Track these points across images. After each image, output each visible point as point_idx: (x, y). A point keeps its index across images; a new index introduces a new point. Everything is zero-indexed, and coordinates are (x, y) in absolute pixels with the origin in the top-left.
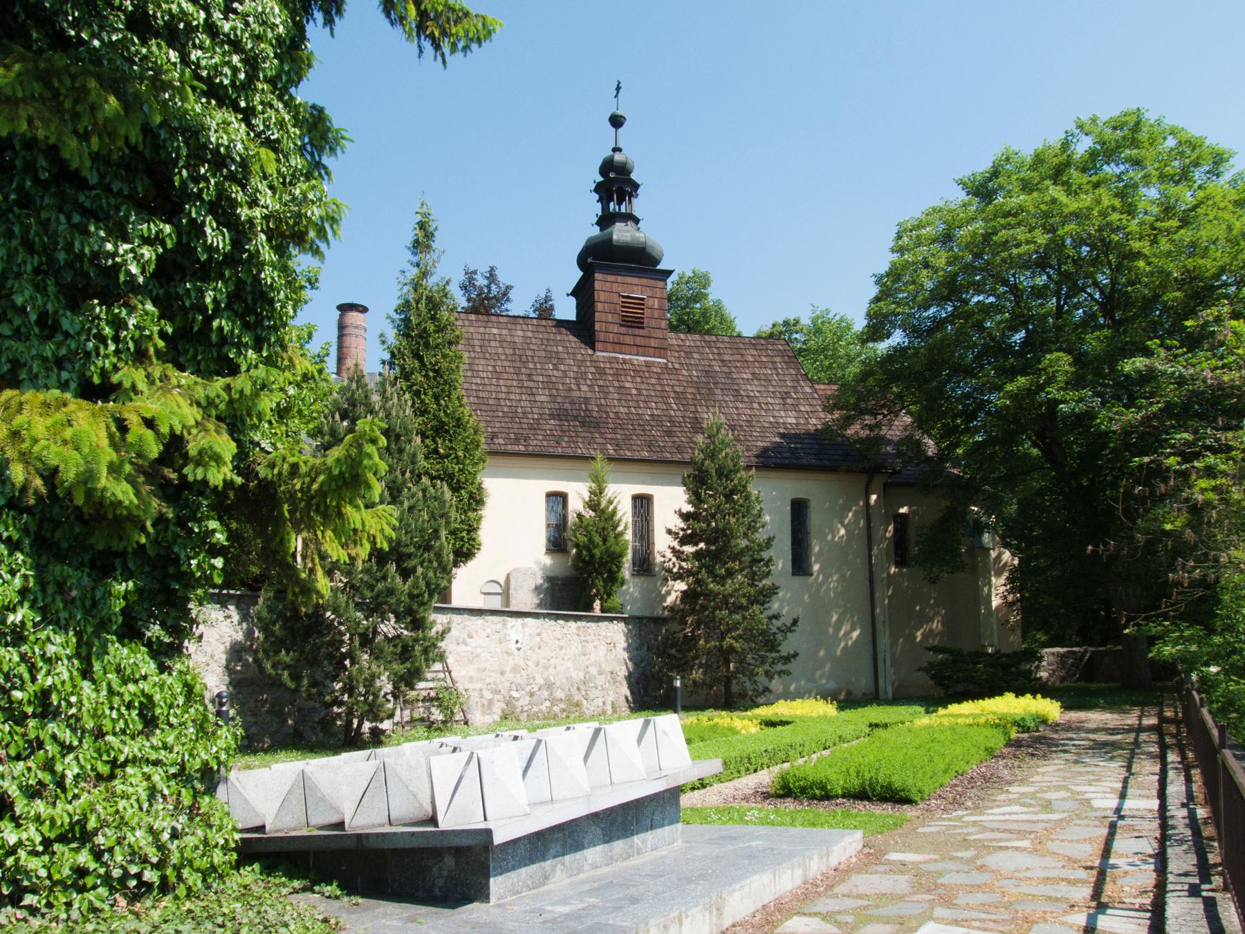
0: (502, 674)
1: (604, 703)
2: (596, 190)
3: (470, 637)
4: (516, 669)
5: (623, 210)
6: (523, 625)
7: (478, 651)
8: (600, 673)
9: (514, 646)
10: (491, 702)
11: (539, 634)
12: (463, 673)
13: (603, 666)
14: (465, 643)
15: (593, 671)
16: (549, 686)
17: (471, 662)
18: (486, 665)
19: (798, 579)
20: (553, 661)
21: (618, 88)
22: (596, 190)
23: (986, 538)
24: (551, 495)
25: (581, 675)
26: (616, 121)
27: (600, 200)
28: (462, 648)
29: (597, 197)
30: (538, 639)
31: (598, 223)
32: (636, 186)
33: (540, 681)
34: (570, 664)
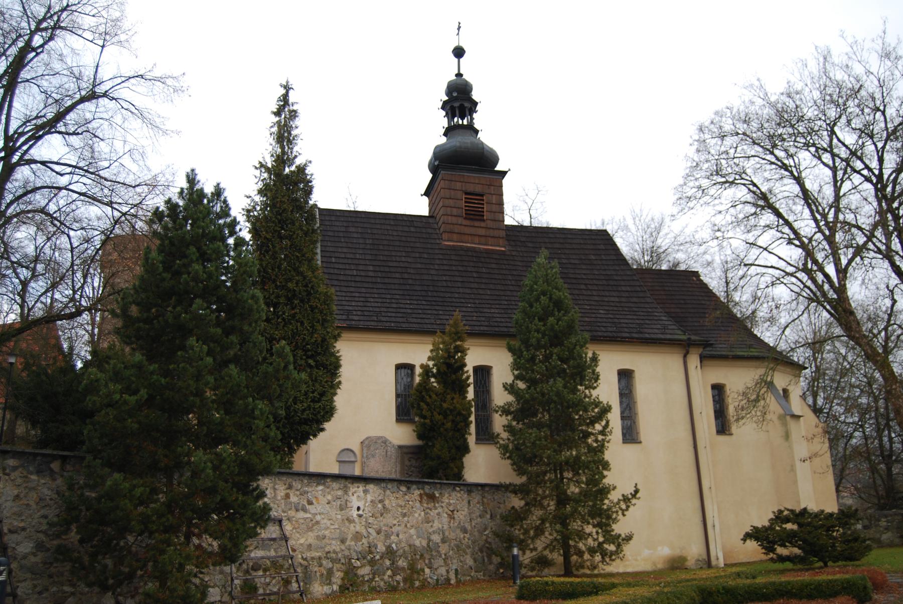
0: (343, 541)
1: (448, 572)
2: (443, 108)
3: (310, 503)
4: (357, 536)
5: (465, 122)
6: (366, 492)
7: (318, 518)
8: (444, 541)
9: (355, 513)
10: (330, 572)
11: (381, 501)
12: (302, 541)
13: (447, 534)
14: (304, 510)
15: (436, 538)
16: (390, 553)
17: (310, 529)
18: (327, 533)
19: (722, 438)
20: (395, 529)
21: (459, 28)
22: (443, 108)
23: (195, 422)
24: (399, 367)
25: (424, 543)
26: (459, 52)
27: (447, 115)
28: (301, 515)
29: (444, 113)
30: (380, 506)
31: (445, 134)
32: (475, 104)
33: (381, 548)
34: (413, 531)
